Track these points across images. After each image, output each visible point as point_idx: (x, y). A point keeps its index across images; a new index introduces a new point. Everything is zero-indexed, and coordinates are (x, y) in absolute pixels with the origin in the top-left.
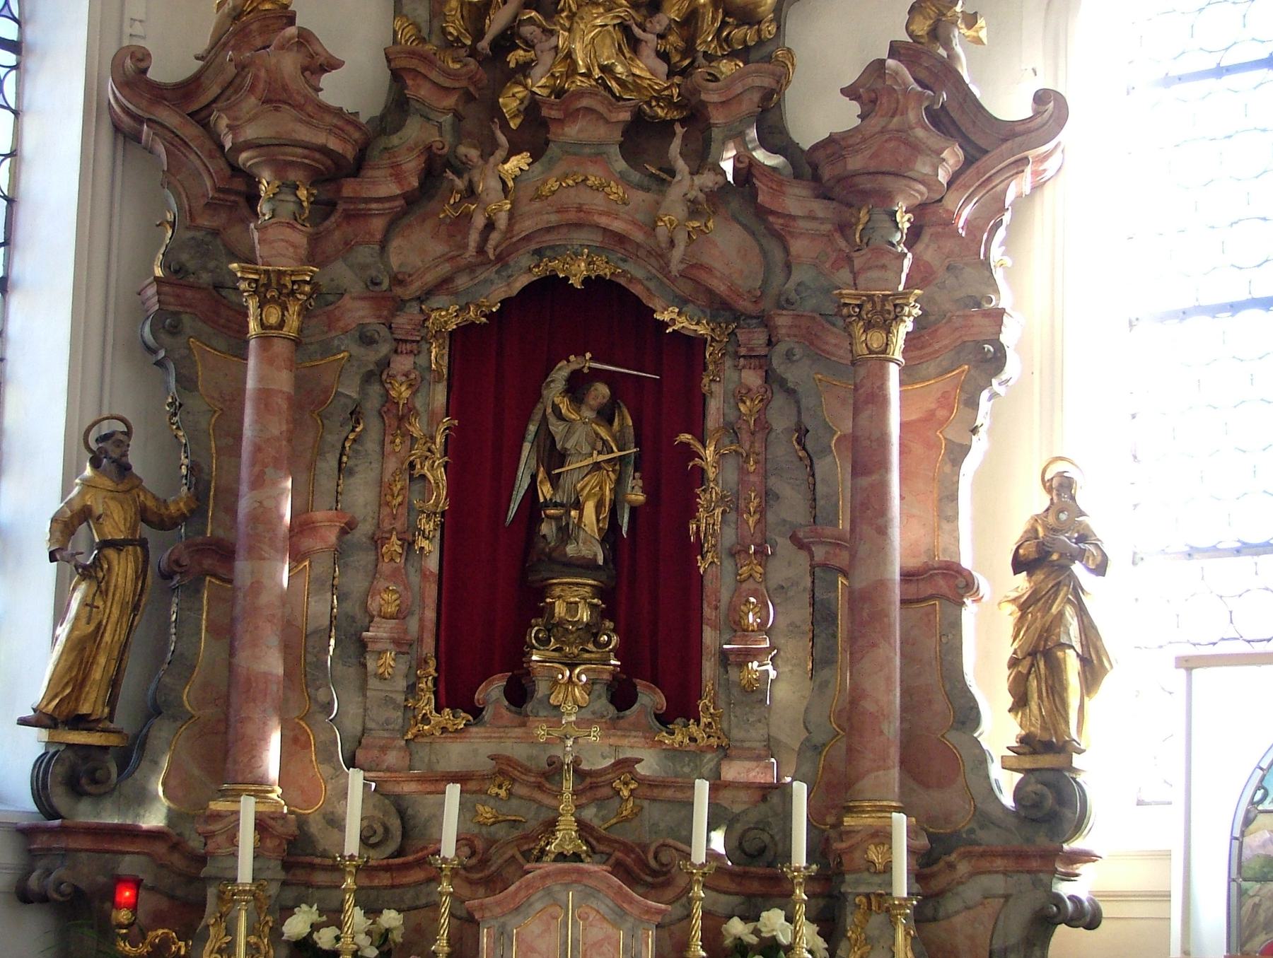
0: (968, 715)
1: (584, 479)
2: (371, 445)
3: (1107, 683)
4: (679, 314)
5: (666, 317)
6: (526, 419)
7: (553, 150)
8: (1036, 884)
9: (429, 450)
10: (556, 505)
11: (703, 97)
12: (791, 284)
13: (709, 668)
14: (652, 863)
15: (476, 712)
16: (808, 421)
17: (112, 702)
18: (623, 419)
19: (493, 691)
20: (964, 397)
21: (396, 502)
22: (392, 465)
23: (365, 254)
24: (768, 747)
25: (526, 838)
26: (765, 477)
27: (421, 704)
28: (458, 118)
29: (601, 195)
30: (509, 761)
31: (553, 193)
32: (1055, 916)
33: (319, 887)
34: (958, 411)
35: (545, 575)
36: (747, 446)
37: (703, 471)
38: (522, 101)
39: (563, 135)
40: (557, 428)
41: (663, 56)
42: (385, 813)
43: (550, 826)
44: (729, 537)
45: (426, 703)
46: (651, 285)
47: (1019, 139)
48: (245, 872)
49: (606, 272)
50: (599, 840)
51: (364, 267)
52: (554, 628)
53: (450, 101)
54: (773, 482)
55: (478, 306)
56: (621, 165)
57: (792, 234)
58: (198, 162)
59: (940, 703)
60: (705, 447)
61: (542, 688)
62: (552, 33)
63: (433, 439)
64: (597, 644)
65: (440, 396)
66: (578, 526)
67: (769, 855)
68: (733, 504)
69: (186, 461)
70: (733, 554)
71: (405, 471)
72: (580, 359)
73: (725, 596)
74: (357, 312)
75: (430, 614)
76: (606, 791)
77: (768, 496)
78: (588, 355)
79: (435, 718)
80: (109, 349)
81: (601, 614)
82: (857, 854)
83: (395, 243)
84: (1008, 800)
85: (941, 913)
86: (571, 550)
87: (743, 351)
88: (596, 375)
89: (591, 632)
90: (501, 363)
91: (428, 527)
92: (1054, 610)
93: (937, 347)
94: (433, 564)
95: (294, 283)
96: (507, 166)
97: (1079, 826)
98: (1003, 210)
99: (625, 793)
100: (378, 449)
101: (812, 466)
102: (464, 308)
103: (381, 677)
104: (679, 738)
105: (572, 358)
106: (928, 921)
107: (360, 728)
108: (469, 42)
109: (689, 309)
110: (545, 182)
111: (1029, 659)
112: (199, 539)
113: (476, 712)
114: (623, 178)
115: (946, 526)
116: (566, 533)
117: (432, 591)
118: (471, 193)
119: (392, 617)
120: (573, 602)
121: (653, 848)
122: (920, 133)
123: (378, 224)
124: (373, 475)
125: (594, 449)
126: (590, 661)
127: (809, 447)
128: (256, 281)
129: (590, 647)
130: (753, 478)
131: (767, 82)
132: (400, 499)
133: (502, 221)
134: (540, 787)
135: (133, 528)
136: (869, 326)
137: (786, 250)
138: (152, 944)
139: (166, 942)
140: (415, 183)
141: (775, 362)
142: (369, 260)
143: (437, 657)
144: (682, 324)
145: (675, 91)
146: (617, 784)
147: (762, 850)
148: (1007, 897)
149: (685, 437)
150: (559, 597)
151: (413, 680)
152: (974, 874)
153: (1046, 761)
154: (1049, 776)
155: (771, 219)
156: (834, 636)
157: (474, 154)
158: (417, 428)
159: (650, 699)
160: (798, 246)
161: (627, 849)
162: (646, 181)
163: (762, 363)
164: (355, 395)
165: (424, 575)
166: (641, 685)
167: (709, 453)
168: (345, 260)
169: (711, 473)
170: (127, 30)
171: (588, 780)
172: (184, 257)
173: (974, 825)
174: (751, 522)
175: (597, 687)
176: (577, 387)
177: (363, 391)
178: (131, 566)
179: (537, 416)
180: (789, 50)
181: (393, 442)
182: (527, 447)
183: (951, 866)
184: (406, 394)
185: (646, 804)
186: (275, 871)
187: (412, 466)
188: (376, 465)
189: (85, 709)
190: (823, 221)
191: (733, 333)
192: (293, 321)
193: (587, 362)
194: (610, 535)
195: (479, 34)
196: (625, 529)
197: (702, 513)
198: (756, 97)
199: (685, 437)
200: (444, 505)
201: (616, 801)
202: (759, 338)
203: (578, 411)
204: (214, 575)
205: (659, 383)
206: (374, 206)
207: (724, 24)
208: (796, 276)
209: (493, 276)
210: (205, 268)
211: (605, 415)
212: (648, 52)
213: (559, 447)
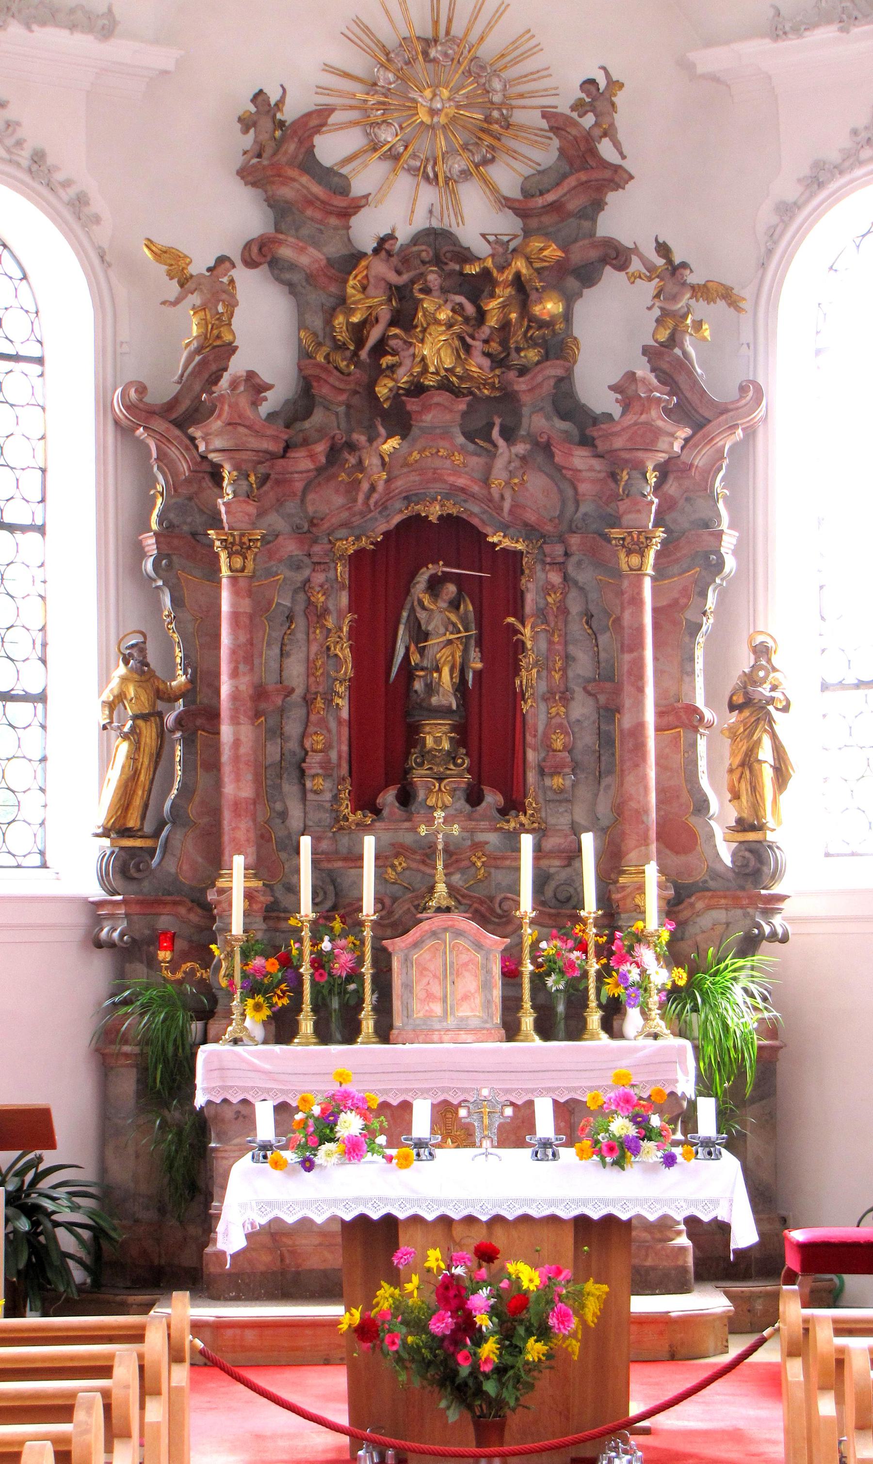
0: (702, 806)
1: (442, 651)
2: (301, 636)
3: (791, 784)
4: (504, 537)
5: (495, 539)
6: (402, 608)
7: (415, 431)
8: (746, 915)
9: (339, 637)
10: (422, 669)
11: (516, 388)
12: (579, 515)
13: (532, 777)
14: (499, 911)
15: (377, 812)
16: (593, 608)
17: (143, 817)
18: (466, 606)
19: (388, 797)
20: (698, 589)
21: (318, 673)
22: (314, 648)
23: (291, 506)
24: (573, 828)
25: (416, 897)
26: (566, 644)
27: (342, 808)
28: (349, 406)
29: (448, 462)
30: (402, 846)
31: (416, 461)
32: (757, 936)
33: (283, 932)
34: (695, 600)
35: (417, 718)
36: (552, 625)
37: (523, 643)
38: (391, 390)
39: (422, 421)
40: (422, 615)
41: (487, 355)
42: (323, 882)
43: (431, 889)
44: (542, 687)
45: (345, 808)
46: (484, 517)
47: (731, 414)
48: (237, 927)
49: (454, 511)
50: (463, 896)
51: (290, 516)
52: (425, 754)
53: (343, 398)
54: (572, 649)
55: (368, 537)
56: (461, 440)
57: (578, 480)
58: (177, 453)
59: (685, 796)
60: (524, 626)
61: (421, 794)
62: (411, 344)
63: (341, 629)
64: (456, 765)
65: (344, 599)
66: (439, 684)
67: (573, 902)
68: (544, 665)
69: (180, 655)
70: (545, 700)
71: (323, 658)
72: (436, 566)
73: (541, 728)
74: (290, 547)
75: (345, 748)
76: (465, 863)
77: (568, 658)
78: (441, 563)
79: (352, 818)
80: (121, 582)
81: (457, 743)
82: (629, 901)
83: (311, 497)
84: (727, 860)
85: (687, 935)
86: (434, 700)
87: (548, 560)
88: (447, 578)
89: (452, 757)
90: (383, 574)
91: (341, 689)
92: (755, 737)
93: (679, 555)
94: (345, 714)
95: (250, 540)
96: (385, 447)
97: (775, 876)
98: (722, 458)
99: (479, 864)
100: (305, 637)
101: (596, 639)
102: (358, 538)
103: (316, 792)
104: (512, 824)
105: (430, 566)
106: (678, 940)
107: (302, 825)
108: (352, 348)
109: (511, 531)
110: (410, 454)
111: (740, 769)
112: (193, 707)
113: (377, 812)
114: (462, 449)
115: (686, 679)
116: (431, 688)
117: (345, 731)
118: (360, 466)
119: (321, 751)
120: (437, 736)
121: (498, 899)
122: (660, 423)
123: (299, 486)
124: (302, 655)
125: (447, 630)
126: (451, 776)
127: (594, 627)
128: (225, 540)
129: (452, 767)
130: (558, 647)
131: (560, 372)
132: (321, 671)
133: (381, 486)
134: (423, 862)
135: (154, 705)
136: (629, 552)
137: (575, 489)
138: (185, 972)
139: (193, 971)
140: (323, 460)
141: (571, 569)
142: (293, 511)
143: (350, 776)
144: (507, 543)
145: (497, 381)
146: (474, 859)
147: (569, 899)
148: (728, 924)
149: (511, 620)
150: (429, 733)
151: (335, 792)
152: (709, 908)
153: (751, 836)
154: (753, 845)
155: (564, 471)
156: (613, 754)
157: (363, 439)
158: (330, 623)
159: (492, 798)
160: (583, 488)
161: (482, 902)
162: (478, 450)
163: (561, 567)
164: (289, 604)
165: (340, 722)
166: (486, 790)
167: (528, 631)
168: (277, 511)
169: (529, 644)
170: (119, 350)
171: (454, 857)
172: (171, 516)
173: (707, 878)
174: (557, 676)
175: (457, 792)
176: (434, 585)
177: (293, 600)
178: (154, 730)
179: (408, 606)
180: (575, 339)
181: (314, 632)
182: (402, 628)
183: (692, 905)
184: (322, 599)
185: (492, 870)
186: (260, 924)
187: (328, 648)
188: (304, 649)
189: (131, 824)
190: (599, 472)
191: (541, 547)
192: (250, 565)
193: (440, 568)
194: (461, 687)
195: (360, 343)
196: (470, 683)
197: (524, 673)
198: (552, 382)
199: (511, 620)
200: (350, 673)
201: (473, 869)
202: (559, 550)
203: (435, 603)
204: (203, 730)
205: (495, 589)
206: (296, 475)
207: (529, 328)
208: (583, 509)
209: (378, 516)
210: (185, 523)
211: (455, 605)
212: (477, 354)
213: (423, 627)
